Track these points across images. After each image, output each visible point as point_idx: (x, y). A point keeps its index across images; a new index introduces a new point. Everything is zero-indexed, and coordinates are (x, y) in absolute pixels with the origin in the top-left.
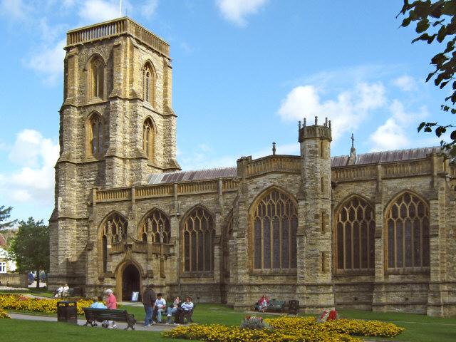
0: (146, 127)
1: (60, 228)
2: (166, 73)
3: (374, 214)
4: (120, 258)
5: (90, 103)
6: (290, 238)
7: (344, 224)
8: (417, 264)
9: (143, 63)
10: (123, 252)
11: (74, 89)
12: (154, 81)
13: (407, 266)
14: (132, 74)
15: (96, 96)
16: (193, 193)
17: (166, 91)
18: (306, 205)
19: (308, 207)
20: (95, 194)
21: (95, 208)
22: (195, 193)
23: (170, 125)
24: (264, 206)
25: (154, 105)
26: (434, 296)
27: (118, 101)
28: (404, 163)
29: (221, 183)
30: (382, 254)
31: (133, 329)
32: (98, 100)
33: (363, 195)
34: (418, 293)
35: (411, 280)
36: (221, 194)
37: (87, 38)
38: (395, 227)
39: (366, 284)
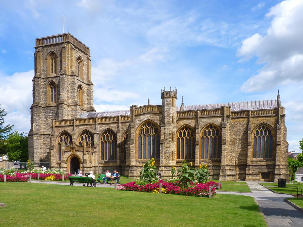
0: (79, 90)
1: (34, 138)
3: (195, 134)
4: (70, 153)
7: (180, 138)
9: (77, 57)
10: (71, 151)
11: (40, 69)
12: (82, 67)
14: (72, 62)
18: (165, 129)
19: (166, 130)
20: (54, 122)
22: (106, 122)
24: (143, 129)
25: (82, 78)
26: (223, 172)
28: (210, 110)
29: (120, 118)
30: (199, 152)
33: (190, 125)
36: (120, 123)
37: (46, 43)
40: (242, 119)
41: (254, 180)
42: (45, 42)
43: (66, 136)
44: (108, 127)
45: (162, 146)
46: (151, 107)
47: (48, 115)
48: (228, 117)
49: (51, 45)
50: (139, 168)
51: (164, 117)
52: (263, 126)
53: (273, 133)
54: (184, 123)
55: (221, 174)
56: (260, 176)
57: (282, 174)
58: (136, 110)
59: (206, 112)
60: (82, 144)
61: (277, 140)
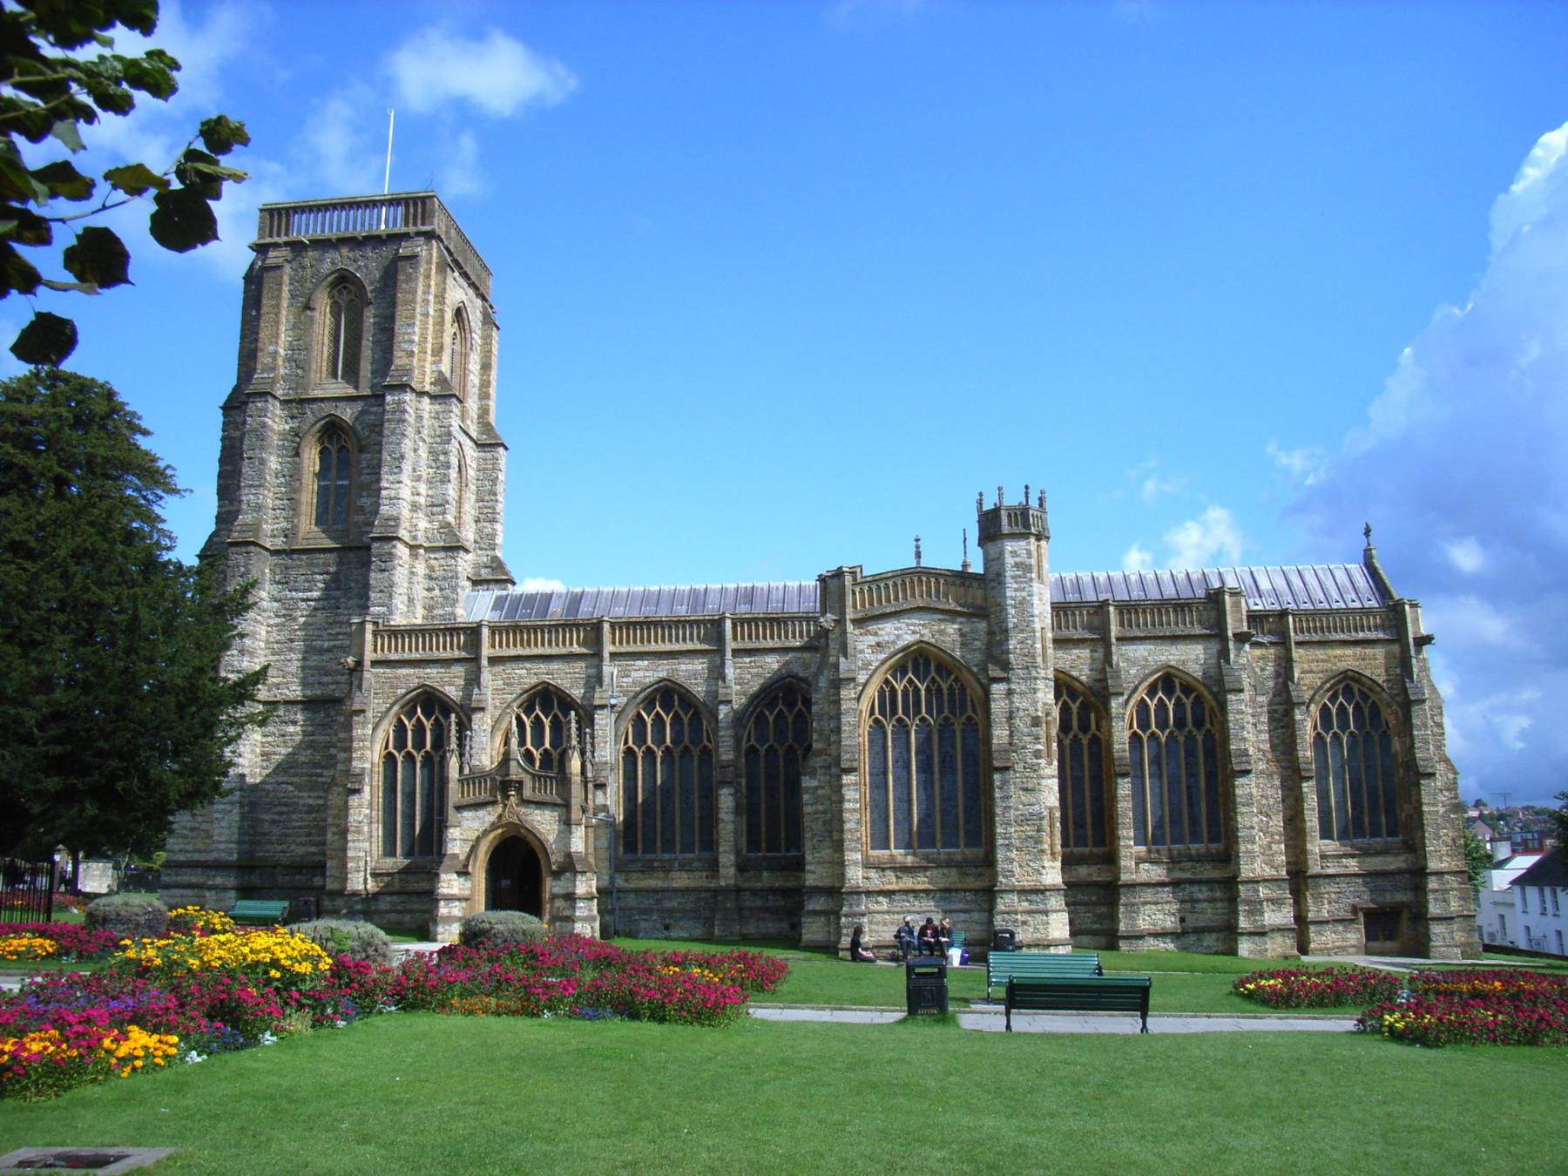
2: (487, 339)
4: (488, 816)
5: (318, 393)
8: (1195, 838)
10: (494, 803)
11: (276, 352)
12: (466, 356)
13: (1173, 842)
15: (335, 376)
16: (646, 648)
17: (485, 384)
18: (1010, 693)
21: (366, 675)
23: (495, 468)
26: (1250, 913)
27: (408, 397)
28: (1162, 605)
32: (341, 388)
33: (1075, 673)
34: (1205, 905)
35: (1188, 875)
39: (1095, 884)
43: (428, 716)
44: (663, 674)
45: (1005, 782)
46: (933, 580)
48: (1241, 638)
49: (342, 241)
50: (880, 899)
51: (1006, 631)
52: (1347, 685)
53: (1392, 722)
55: (1243, 923)
58: (857, 590)
59: (1144, 612)
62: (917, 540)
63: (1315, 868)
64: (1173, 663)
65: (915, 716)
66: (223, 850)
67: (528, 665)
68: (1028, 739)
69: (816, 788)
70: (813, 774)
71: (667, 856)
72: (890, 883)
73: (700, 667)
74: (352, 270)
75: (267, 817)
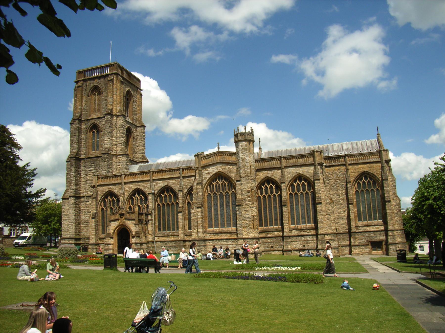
6: (231, 206)
10: (118, 220)
22: (164, 177)
28: (297, 157)
31: (160, 273)
33: (273, 177)
38: (294, 198)
40: (337, 168)
41: (363, 254)
42: (87, 75)
44: (166, 184)
47: (89, 169)
50: (210, 241)
54: (265, 175)
56: (369, 248)
57: (398, 243)
60: (133, 209)
61: (386, 195)
62: (218, 144)
63: (354, 230)
64: (301, 173)
65: (219, 191)
66: (71, 234)
67: (134, 184)
68: (246, 197)
69: (194, 212)
70: (193, 209)
71: (168, 232)
72: (212, 237)
73: (175, 181)
74: (97, 85)
75: (83, 225)
